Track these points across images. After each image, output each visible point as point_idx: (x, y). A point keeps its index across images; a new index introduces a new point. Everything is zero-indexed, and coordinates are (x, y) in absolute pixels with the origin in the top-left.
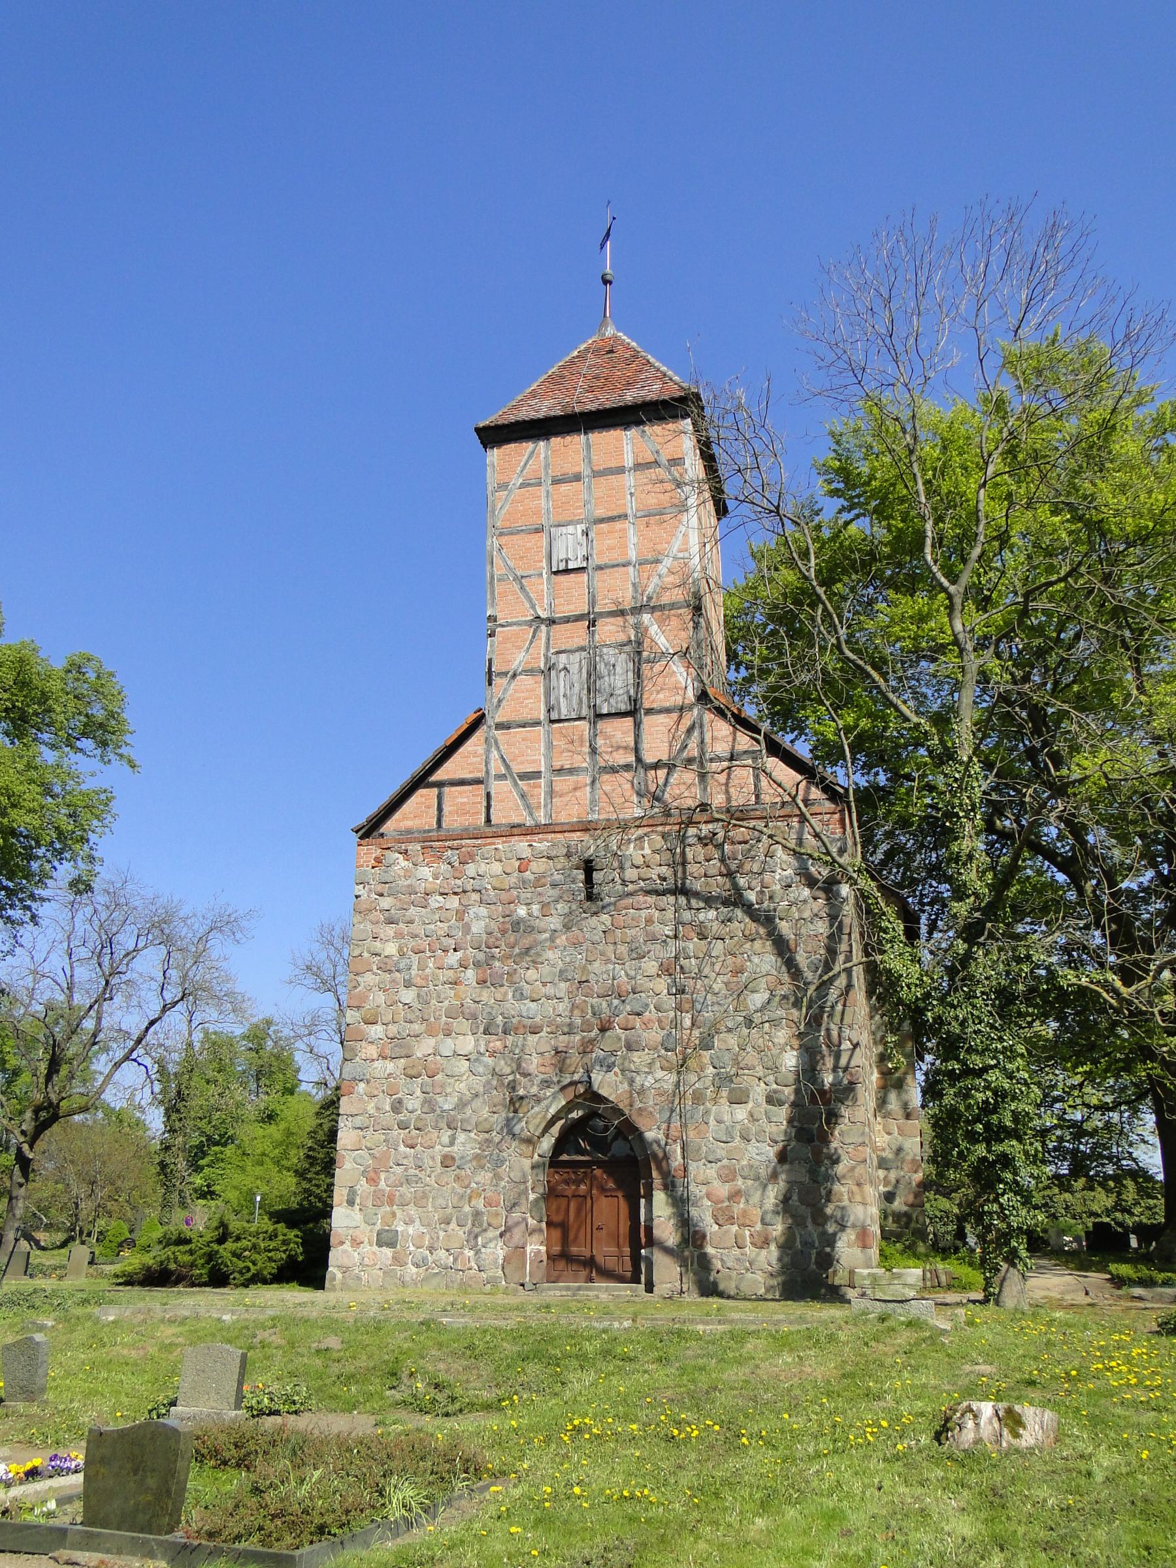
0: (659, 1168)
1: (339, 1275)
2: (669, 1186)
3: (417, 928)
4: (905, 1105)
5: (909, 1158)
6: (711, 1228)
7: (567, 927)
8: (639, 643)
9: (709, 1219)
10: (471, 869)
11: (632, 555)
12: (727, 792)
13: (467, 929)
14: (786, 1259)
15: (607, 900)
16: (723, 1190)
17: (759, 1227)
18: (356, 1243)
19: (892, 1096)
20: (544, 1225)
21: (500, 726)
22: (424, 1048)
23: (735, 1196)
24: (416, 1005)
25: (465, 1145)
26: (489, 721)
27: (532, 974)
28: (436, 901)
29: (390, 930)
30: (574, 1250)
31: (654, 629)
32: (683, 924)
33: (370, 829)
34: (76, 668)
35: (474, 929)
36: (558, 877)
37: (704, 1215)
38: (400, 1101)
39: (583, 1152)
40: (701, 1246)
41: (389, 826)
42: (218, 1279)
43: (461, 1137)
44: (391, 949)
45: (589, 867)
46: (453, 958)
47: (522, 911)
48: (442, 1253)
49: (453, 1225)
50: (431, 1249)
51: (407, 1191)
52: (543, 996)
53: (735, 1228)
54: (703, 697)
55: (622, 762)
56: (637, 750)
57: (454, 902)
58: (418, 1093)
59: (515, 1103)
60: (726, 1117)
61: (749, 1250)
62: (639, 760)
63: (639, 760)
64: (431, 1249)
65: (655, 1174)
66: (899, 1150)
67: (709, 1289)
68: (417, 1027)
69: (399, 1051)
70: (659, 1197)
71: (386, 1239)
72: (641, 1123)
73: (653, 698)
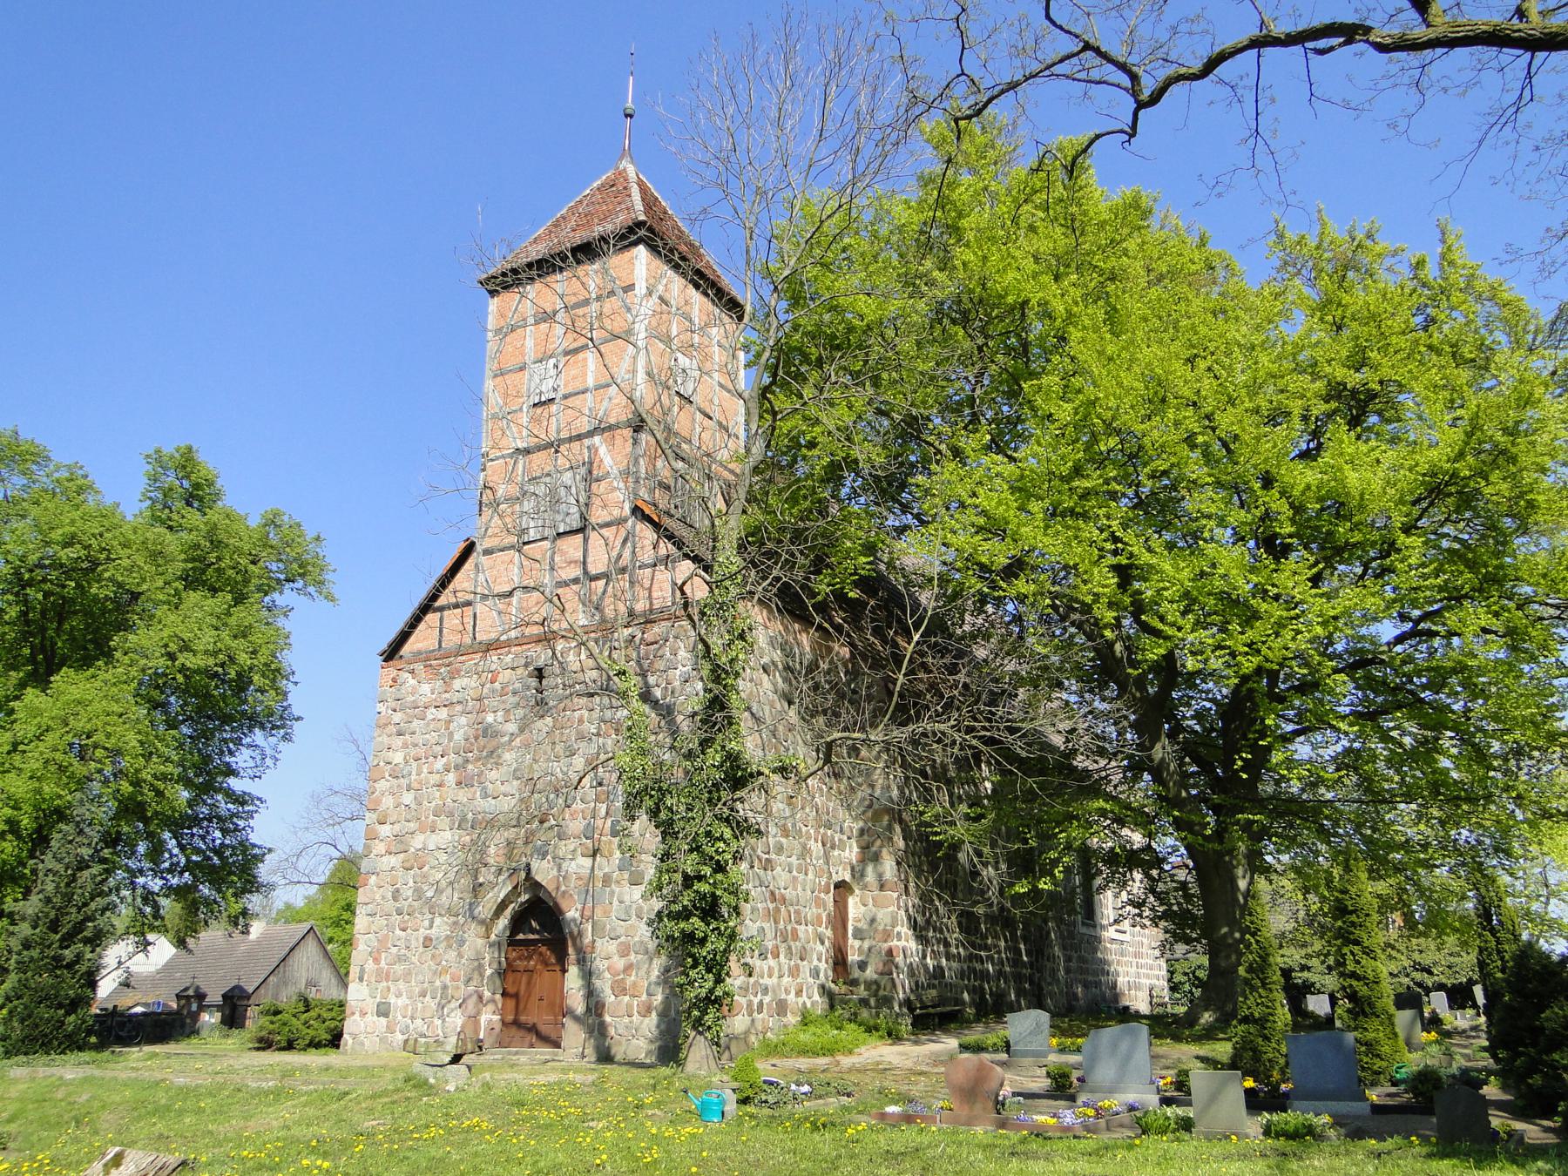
0: (574, 944)
1: (350, 1042)
2: (581, 962)
3: (419, 738)
4: (880, 876)
5: (881, 928)
6: (610, 999)
7: (522, 730)
8: (591, 463)
9: (608, 991)
10: (457, 684)
11: (590, 383)
12: (650, 597)
13: (451, 734)
14: (663, 1027)
15: (551, 703)
16: (620, 963)
17: (644, 996)
18: (363, 1014)
19: (870, 869)
20: (498, 996)
21: (487, 552)
22: (417, 842)
23: (628, 969)
24: (413, 806)
25: (441, 927)
26: (479, 548)
27: (493, 775)
28: (431, 713)
29: (399, 741)
30: (523, 1018)
31: (603, 450)
32: (605, 722)
33: (392, 653)
34: (272, 522)
35: (456, 737)
36: (518, 685)
37: (604, 985)
38: (398, 890)
39: (533, 931)
40: (600, 1015)
41: (406, 649)
42: (289, 1046)
43: (438, 921)
44: (398, 758)
45: (540, 674)
46: (440, 764)
47: (490, 718)
48: (419, 1022)
49: (428, 997)
50: (413, 1018)
51: (399, 968)
52: (501, 793)
53: (627, 998)
54: (636, 510)
55: (572, 576)
56: (584, 563)
57: (443, 713)
58: (411, 883)
59: (477, 889)
60: (626, 898)
61: (636, 1017)
62: (586, 572)
63: (586, 572)
64: (413, 1018)
65: (570, 950)
66: (873, 920)
67: (605, 1057)
68: (412, 826)
69: (402, 848)
70: (573, 971)
71: (383, 1011)
72: (564, 904)
73: (598, 515)
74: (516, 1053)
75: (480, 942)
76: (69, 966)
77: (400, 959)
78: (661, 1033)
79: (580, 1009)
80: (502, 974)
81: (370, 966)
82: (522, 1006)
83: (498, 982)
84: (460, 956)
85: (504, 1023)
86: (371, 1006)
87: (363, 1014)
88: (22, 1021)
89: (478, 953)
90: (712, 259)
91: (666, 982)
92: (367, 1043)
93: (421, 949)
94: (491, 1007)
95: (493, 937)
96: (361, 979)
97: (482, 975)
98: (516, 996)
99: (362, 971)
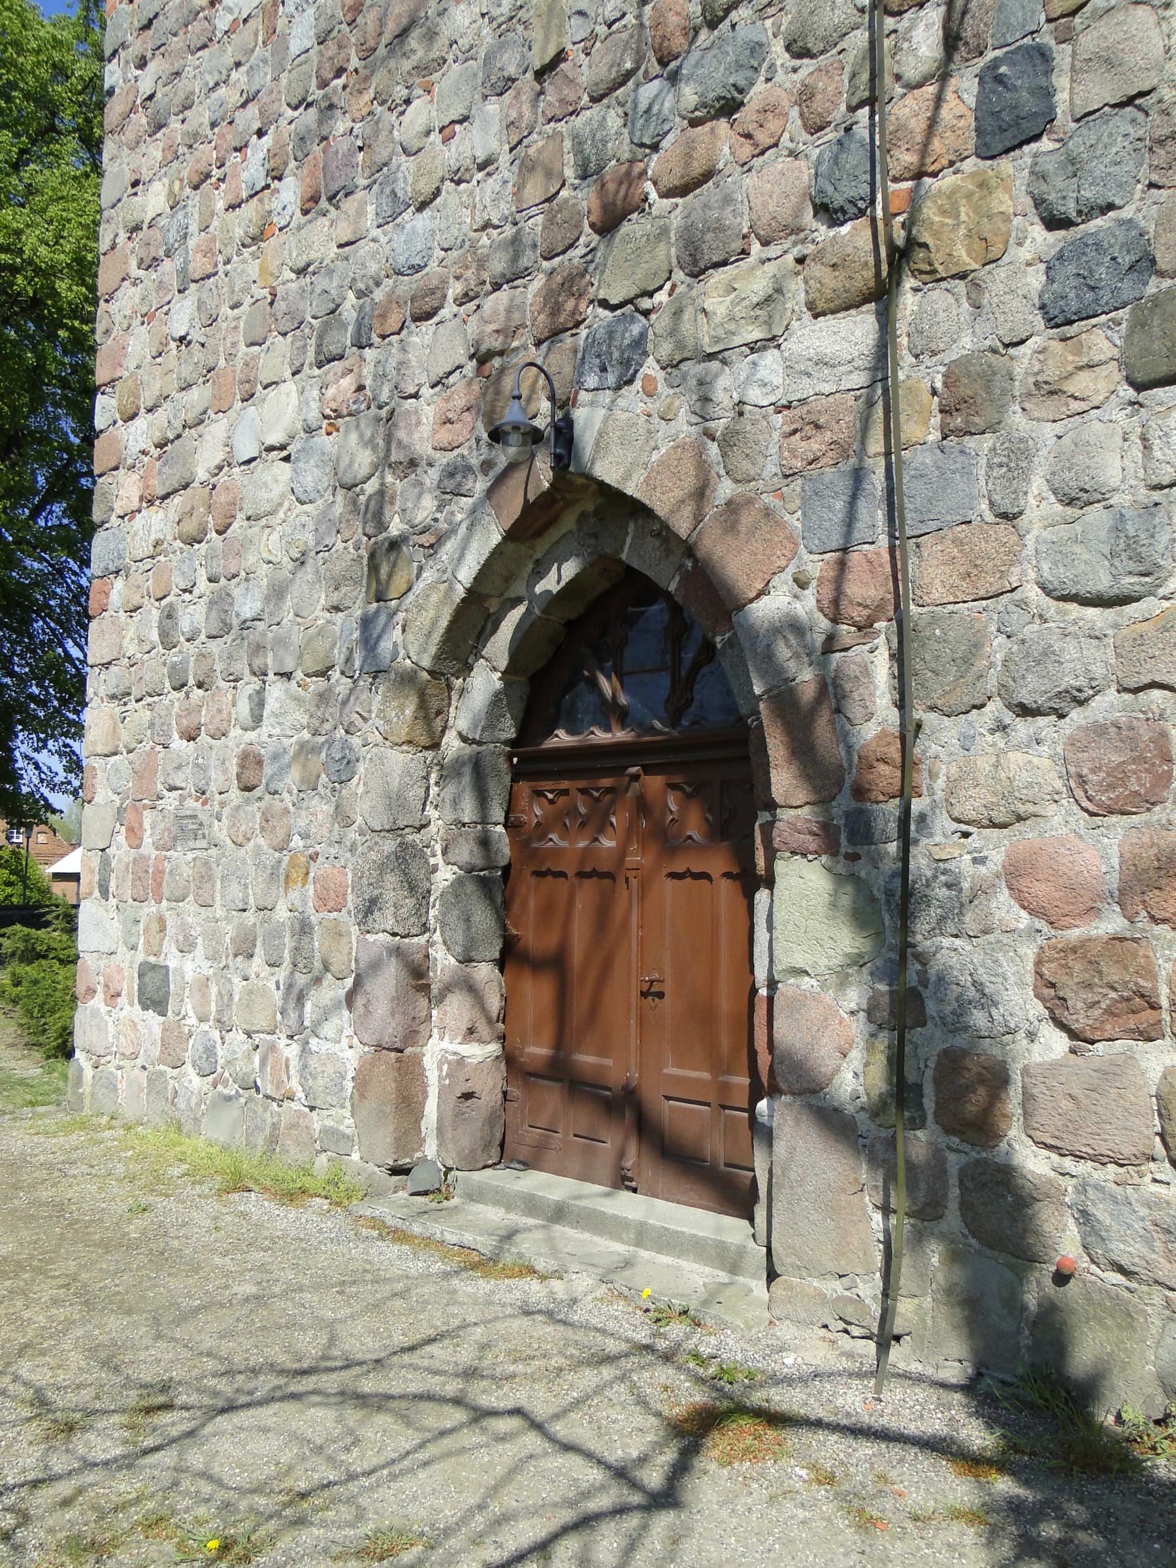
0: (803, 751)
1: (88, 1072)
2: (848, 835)
9: (1020, 1003)
20: (485, 972)
37: (997, 963)
40: (981, 1129)
49: (258, 963)
50: (225, 1028)
51: (183, 858)
65: (784, 781)
71: (154, 998)
77: (187, 829)
80: (495, 883)
81: (121, 851)
83: (483, 918)
84: (342, 817)
85: (510, 1060)
86: (125, 971)
95: (451, 744)
96: (105, 893)
97: (418, 891)
98: (555, 964)
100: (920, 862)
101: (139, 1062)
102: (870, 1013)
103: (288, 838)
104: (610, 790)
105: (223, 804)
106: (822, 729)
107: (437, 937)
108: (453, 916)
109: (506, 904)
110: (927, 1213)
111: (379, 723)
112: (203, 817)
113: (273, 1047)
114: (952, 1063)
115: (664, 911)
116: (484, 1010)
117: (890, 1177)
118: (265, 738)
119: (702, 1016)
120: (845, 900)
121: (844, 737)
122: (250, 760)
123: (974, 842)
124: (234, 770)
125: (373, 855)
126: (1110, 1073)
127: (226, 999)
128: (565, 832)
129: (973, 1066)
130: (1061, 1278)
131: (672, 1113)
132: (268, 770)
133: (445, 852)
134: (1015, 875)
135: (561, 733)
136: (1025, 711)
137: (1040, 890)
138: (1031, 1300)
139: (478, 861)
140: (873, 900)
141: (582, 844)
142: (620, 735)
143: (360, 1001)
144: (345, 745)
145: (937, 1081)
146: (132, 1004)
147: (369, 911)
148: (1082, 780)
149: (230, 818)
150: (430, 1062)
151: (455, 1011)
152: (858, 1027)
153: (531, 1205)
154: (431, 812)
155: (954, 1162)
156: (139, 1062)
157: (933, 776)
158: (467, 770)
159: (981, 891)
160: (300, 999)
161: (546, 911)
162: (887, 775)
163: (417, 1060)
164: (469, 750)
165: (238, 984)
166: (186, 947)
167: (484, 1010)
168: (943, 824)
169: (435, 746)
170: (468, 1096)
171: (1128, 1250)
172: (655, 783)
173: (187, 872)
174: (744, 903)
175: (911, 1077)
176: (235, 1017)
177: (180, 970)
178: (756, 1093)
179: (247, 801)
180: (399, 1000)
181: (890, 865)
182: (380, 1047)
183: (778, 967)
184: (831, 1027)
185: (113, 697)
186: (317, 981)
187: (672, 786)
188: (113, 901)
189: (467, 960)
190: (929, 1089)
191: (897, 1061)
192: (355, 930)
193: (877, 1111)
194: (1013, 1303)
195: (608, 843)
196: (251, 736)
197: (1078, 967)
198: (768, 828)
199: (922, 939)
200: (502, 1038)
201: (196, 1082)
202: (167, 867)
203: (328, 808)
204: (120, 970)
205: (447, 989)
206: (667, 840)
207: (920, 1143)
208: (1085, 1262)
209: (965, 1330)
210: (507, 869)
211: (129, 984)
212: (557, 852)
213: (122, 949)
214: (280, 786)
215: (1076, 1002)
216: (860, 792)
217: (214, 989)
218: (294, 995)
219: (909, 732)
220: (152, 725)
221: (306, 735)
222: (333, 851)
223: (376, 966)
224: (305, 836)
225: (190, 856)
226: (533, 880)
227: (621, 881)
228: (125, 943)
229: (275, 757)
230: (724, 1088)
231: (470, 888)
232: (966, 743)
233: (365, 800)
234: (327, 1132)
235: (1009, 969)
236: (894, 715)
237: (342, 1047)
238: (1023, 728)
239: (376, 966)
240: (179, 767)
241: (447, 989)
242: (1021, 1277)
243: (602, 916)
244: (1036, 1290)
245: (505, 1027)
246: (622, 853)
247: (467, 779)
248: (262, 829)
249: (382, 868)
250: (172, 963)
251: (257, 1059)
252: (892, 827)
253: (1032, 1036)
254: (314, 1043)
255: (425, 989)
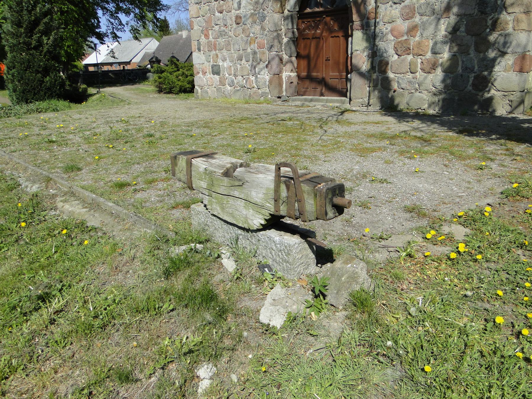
0: (359, 12)
1: (199, 91)
2: (366, 26)
9: (391, 51)
14: (449, 81)
16: (403, 26)
17: (429, 55)
18: (204, 73)
20: (294, 59)
23: (412, 30)
37: (388, 46)
40: (384, 72)
49: (244, 61)
50: (235, 76)
51: (222, 41)
53: (410, 57)
61: (419, 74)
65: (355, 17)
71: (216, 71)
74: (311, 100)
75: (277, 16)
76: (36, 48)
77: (221, 34)
78: (446, 87)
79: (364, 65)
80: (295, 41)
81: (203, 40)
82: (312, 64)
83: (293, 48)
84: (263, 29)
85: (299, 76)
86: (208, 67)
87: (204, 73)
88: (19, 81)
89: (276, 25)
90: (219, 221)
91: (452, 41)
92: (209, 92)
93: (235, 26)
94: (289, 67)
95: (286, 12)
96: (199, 50)
97: (280, 43)
98: (307, 57)
99: (199, 44)
100: (377, 30)
101: (214, 86)
102: (368, 56)
103: (250, 34)
104: (319, 21)
105: (231, 28)
106: (362, 7)
107: (284, 52)
108: (287, 48)
109: (297, 45)
110: (375, 87)
111: (272, 8)
112: (227, 31)
113: (249, 78)
114: (381, 62)
115: (330, 45)
116: (294, 66)
117: (370, 82)
118: (242, 12)
119: (337, 63)
120: (365, 38)
121: (365, 9)
122: (238, 17)
123: (386, 26)
124: (234, 20)
125: (271, 36)
126: (403, 60)
127: (236, 70)
128: (309, 30)
129: (384, 62)
130: (394, 91)
131: (331, 82)
132: (243, 19)
133: (285, 35)
134: (392, 31)
135: (308, 9)
136: (395, 3)
137: (395, 33)
138: (390, 96)
139: (292, 37)
140: (369, 37)
141: (313, 32)
142: (321, 9)
143: (270, 66)
144: (263, 13)
145: (378, 66)
146: (210, 74)
147: (271, 48)
148: (403, 15)
149: (233, 30)
150: (284, 77)
151: (289, 67)
152: (366, 59)
153: (306, 100)
154: (282, 27)
155: (380, 77)
156: (214, 86)
157: (380, 15)
158: (290, 18)
159: (387, 34)
160: (255, 68)
161: (305, 47)
162: (373, 15)
163: (282, 76)
164: (290, 13)
165: (239, 66)
166: (224, 60)
167: (294, 66)
168: (381, 23)
169: (283, 13)
170: (292, 83)
171: (403, 86)
172: (328, 19)
173: (223, 44)
174: (345, 42)
175: (374, 65)
176: (239, 73)
177: (223, 65)
178: (348, 73)
179: (238, 27)
180: (278, 65)
181: (372, 31)
182: (274, 74)
183: (353, 50)
184: (361, 59)
185: (197, 3)
186: (259, 63)
187: (332, 19)
188: (202, 52)
189: (291, 56)
190: (377, 67)
191: (372, 63)
192: (267, 52)
193: (369, 72)
194: (387, 97)
195: (318, 31)
196: (238, 12)
197: (400, 45)
198: (352, 27)
199: (377, 43)
200: (297, 72)
201: (229, 88)
202: (217, 43)
203: (259, 27)
204: (206, 67)
205: (287, 63)
206: (331, 30)
207: (374, 76)
208: (398, 89)
209: (379, 100)
210: (297, 38)
211: (209, 69)
212: (308, 34)
213: (206, 62)
214: (247, 23)
215: (399, 50)
216: (368, 18)
217: (233, 68)
218: (253, 67)
219: (377, 7)
220: (209, 10)
221: (252, 11)
222: (261, 36)
223: (273, 59)
224: (253, 33)
225: (224, 40)
226: (302, 40)
227: (321, 39)
228: (207, 61)
229: (245, 16)
230: (341, 76)
231: (291, 42)
232: (386, 9)
233: (268, 24)
234: (262, 93)
235: (390, 46)
236: (374, 4)
237: (265, 76)
238: (395, 6)
239: (273, 59)
240: (218, 20)
241: (287, 63)
242: (389, 93)
243: (317, 47)
244: (391, 94)
245: (298, 70)
246: (322, 33)
247: (290, 20)
248: (242, 33)
249: (274, 39)
250: (220, 64)
251: (245, 81)
252: (373, 24)
253: (393, 56)
254: (259, 76)
255: (282, 63)
